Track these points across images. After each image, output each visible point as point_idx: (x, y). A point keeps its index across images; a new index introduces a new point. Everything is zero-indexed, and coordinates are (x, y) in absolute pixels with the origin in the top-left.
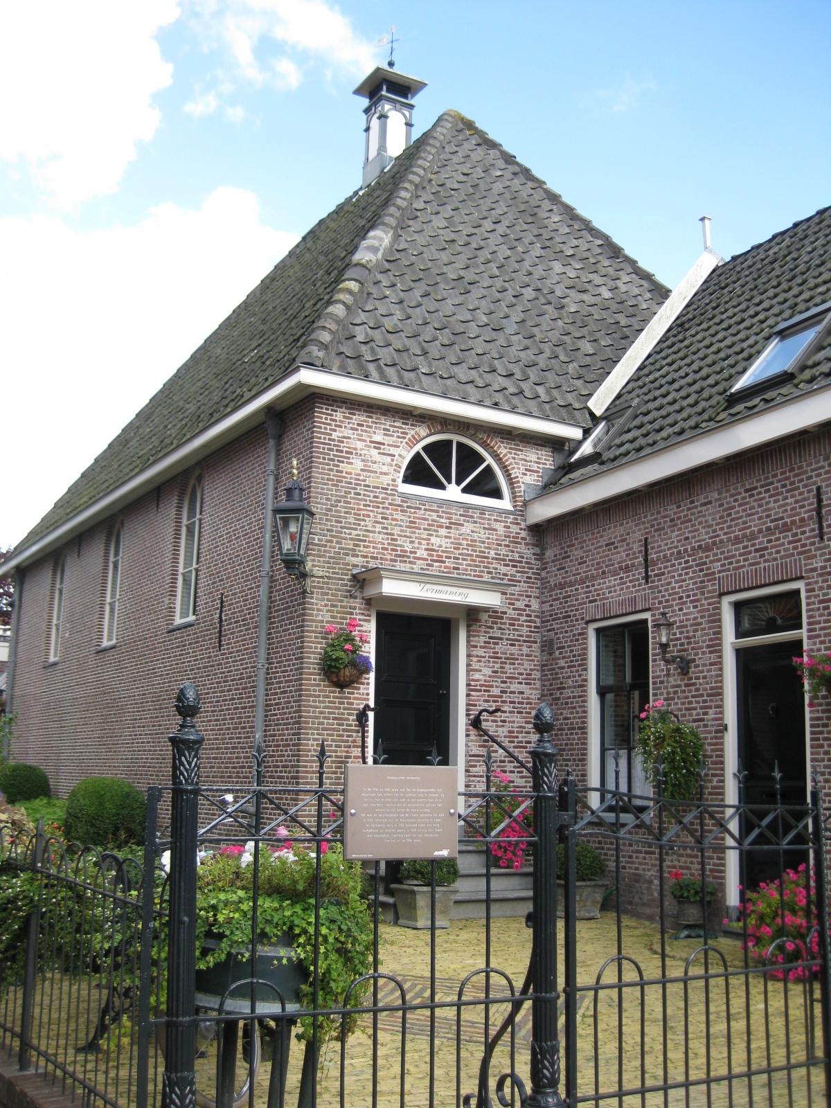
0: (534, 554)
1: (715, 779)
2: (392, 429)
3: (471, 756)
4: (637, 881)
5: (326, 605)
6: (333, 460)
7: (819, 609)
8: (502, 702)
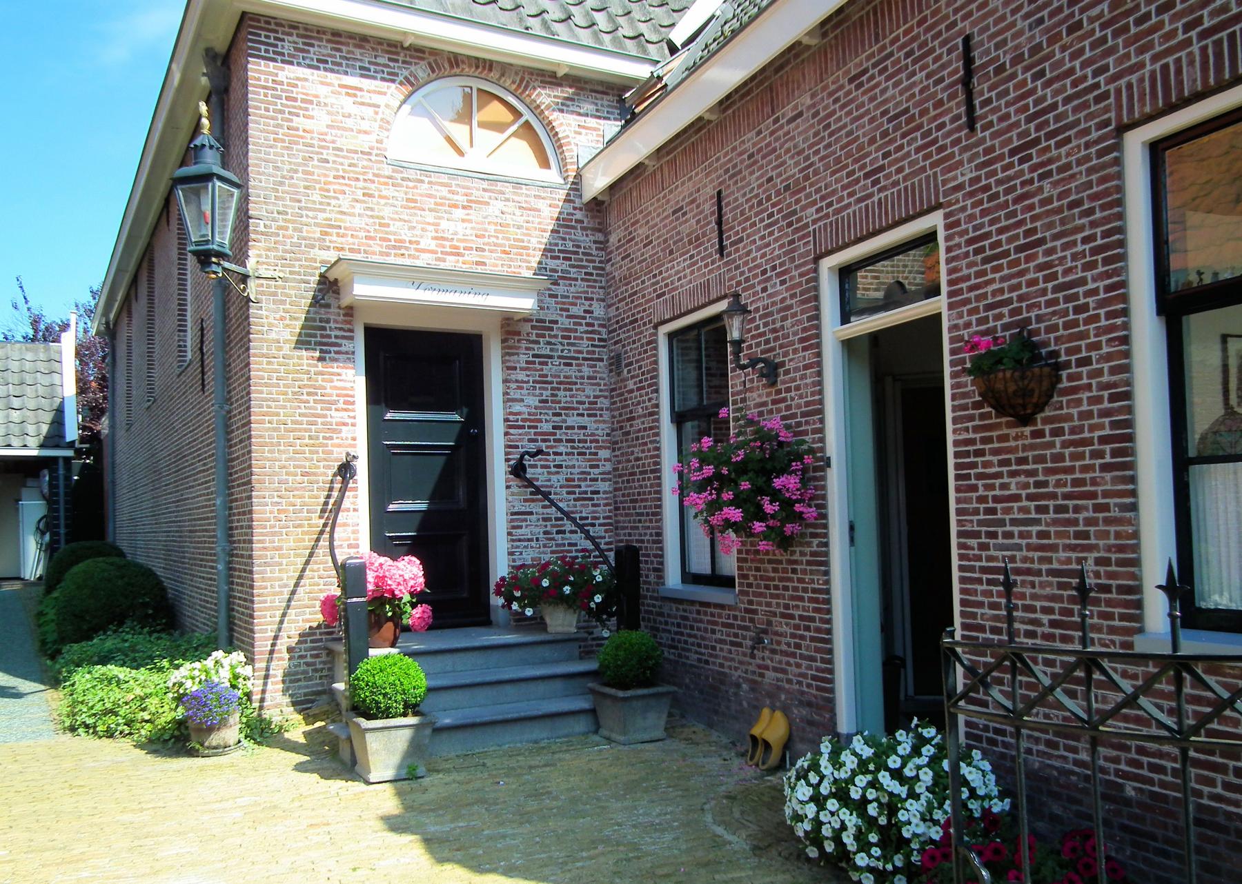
0: (595, 242)
1: (816, 541)
2: (372, 68)
3: (513, 514)
4: (722, 683)
5: (282, 318)
6: (282, 112)
7: (967, 255)
8: (555, 441)
